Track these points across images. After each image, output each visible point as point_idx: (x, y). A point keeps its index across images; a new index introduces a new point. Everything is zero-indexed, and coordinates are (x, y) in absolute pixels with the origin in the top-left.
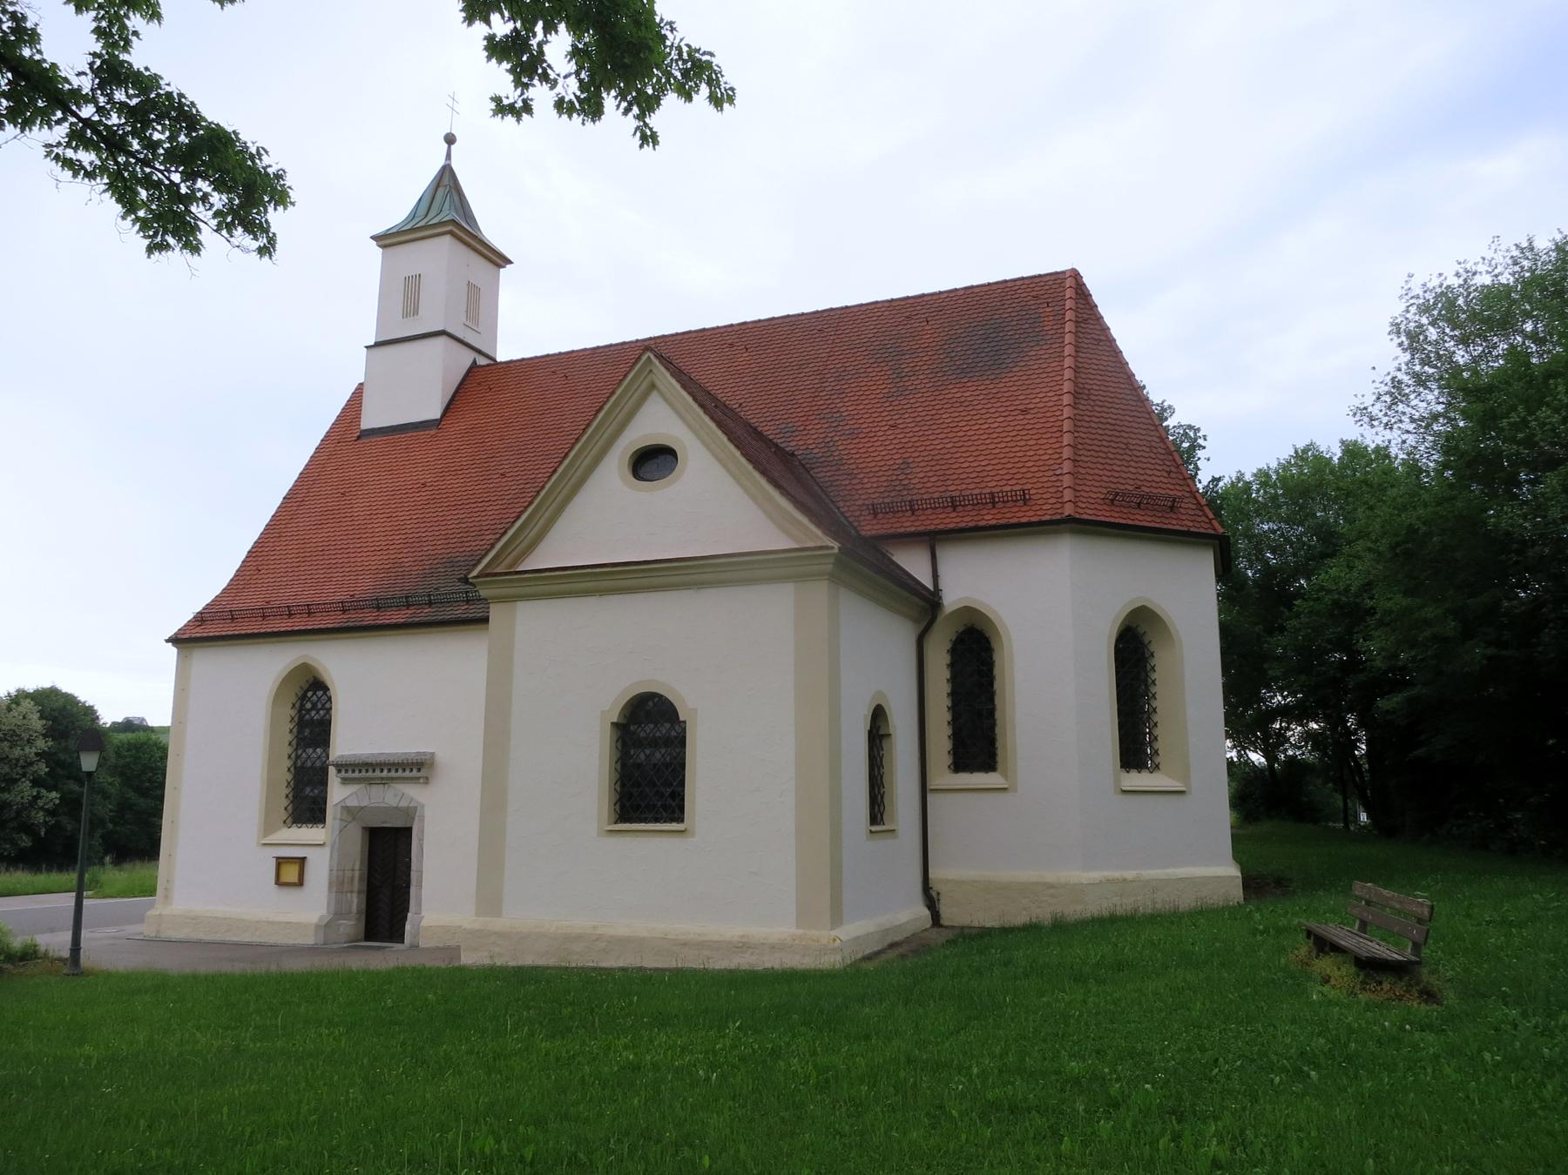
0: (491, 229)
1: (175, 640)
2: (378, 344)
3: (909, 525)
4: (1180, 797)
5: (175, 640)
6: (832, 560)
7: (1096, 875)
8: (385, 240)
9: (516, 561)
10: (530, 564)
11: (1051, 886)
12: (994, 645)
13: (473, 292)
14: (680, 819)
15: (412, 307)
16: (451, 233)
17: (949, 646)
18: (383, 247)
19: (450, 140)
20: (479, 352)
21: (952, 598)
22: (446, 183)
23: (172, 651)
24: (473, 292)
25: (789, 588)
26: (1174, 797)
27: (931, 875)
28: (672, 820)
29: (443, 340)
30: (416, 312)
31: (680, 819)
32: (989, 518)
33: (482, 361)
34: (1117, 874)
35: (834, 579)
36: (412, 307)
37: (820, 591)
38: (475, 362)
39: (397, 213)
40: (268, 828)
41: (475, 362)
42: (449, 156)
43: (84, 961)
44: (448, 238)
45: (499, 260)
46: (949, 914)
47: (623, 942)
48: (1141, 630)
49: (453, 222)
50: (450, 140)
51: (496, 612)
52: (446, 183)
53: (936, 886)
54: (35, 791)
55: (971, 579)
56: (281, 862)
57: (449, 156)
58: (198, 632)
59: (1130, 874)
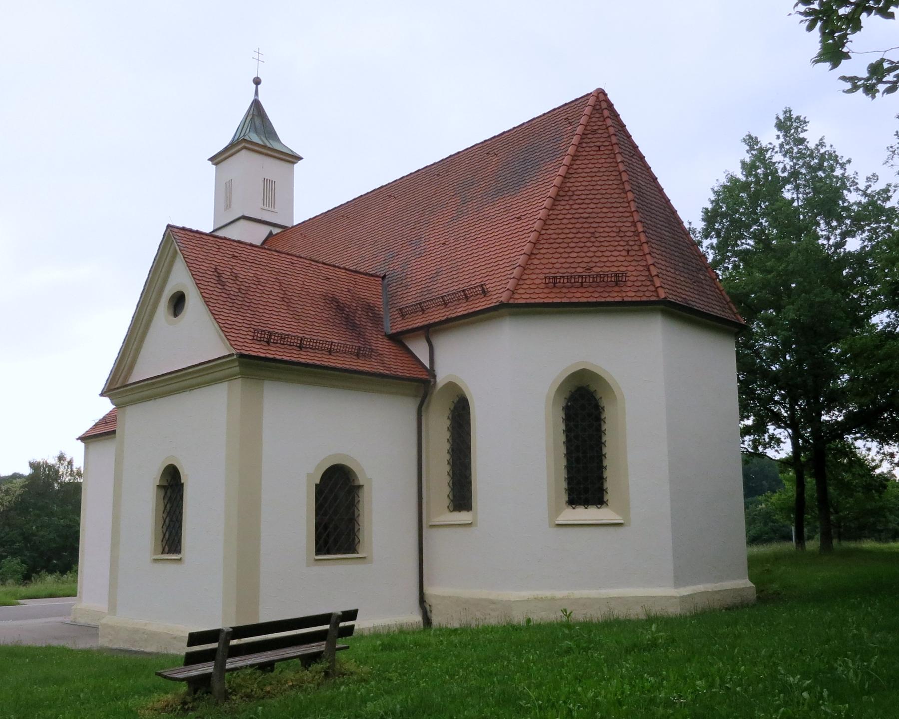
0: (288, 138)
1: (83, 438)
3: (418, 321)
4: (616, 528)
5: (83, 438)
6: (236, 364)
7: (526, 594)
8: (216, 159)
10: (130, 381)
12: (604, 403)
13: (269, 185)
15: (228, 205)
16: (245, 148)
17: (447, 412)
18: (216, 164)
19: (257, 82)
21: (442, 376)
23: (81, 445)
24: (269, 185)
26: (611, 529)
27: (427, 590)
29: (242, 221)
30: (230, 206)
33: (276, 231)
35: (244, 375)
36: (228, 205)
37: (238, 384)
38: (271, 233)
41: (271, 233)
44: (244, 152)
45: (292, 158)
46: (436, 620)
47: (153, 635)
50: (257, 82)
53: (429, 600)
54: (13, 531)
55: (458, 360)
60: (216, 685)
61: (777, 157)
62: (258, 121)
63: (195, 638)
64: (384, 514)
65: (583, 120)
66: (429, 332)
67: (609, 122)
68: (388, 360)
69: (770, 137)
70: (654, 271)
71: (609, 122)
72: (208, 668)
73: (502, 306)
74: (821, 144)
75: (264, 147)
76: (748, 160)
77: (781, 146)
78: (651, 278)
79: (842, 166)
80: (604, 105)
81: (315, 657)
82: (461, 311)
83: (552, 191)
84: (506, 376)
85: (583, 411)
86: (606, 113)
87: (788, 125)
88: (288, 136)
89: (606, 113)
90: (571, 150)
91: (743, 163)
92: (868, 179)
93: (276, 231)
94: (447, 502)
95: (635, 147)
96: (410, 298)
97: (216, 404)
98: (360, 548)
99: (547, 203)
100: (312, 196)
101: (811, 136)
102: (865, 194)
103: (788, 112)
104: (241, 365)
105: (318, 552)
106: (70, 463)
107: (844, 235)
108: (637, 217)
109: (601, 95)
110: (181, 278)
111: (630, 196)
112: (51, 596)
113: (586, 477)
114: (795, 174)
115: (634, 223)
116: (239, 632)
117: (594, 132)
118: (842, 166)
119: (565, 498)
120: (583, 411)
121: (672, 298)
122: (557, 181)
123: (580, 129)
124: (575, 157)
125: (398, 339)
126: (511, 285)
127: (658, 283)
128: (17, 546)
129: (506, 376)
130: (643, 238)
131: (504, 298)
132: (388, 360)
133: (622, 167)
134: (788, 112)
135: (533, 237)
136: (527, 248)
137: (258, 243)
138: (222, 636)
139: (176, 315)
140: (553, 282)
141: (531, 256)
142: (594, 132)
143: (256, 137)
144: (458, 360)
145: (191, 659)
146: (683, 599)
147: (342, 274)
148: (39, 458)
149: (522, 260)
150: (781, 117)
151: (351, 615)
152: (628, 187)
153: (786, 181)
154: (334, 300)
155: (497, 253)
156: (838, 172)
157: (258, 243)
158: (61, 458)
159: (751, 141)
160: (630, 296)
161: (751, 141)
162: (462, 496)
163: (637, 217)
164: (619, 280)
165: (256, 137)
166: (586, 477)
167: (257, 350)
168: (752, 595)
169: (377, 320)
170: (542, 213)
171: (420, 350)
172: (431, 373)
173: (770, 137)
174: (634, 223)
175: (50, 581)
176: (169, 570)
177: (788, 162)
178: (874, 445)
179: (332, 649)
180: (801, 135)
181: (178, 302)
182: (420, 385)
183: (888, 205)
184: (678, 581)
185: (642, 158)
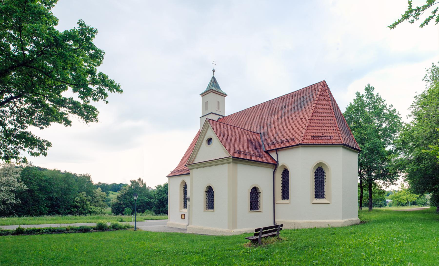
1: (168, 177)
2: (202, 117)
7: (304, 221)
8: (203, 95)
9: (193, 162)
11: (295, 223)
13: (218, 103)
14: (258, 209)
15: (207, 109)
17: (282, 173)
19: (214, 71)
20: (220, 115)
22: (214, 80)
23: (167, 178)
25: (227, 165)
27: (276, 220)
28: (211, 209)
31: (258, 209)
32: (287, 145)
33: (221, 117)
34: (310, 221)
35: (233, 162)
37: (231, 165)
39: (204, 89)
40: (180, 210)
42: (214, 74)
43: (137, 227)
45: (224, 95)
48: (322, 167)
49: (212, 89)
50: (214, 71)
51: (191, 172)
52: (214, 80)
55: (285, 159)
56: (182, 215)
57: (214, 74)
58: (171, 175)
59: (313, 221)
60: (260, 241)
61: (365, 99)
62: (215, 83)
63: (256, 230)
64: (265, 199)
65: (320, 90)
66: (277, 150)
67: (327, 91)
68: (266, 159)
69: (363, 92)
70: (340, 136)
71: (327, 91)
72: (257, 237)
73: (300, 144)
74: (377, 95)
75: (217, 91)
76: (356, 99)
77: (366, 95)
78: (339, 137)
79: (383, 102)
80: (326, 86)
81: (274, 235)
82: (287, 145)
83: (312, 111)
84: (300, 164)
85: (320, 174)
86: (326, 88)
87: (369, 89)
88: (223, 89)
89: (326, 88)
90: (317, 99)
91: (354, 100)
92: (390, 106)
93: (221, 117)
94: (281, 197)
95: (333, 98)
96: (270, 141)
97: (224, 170)
98: (260, 209)
99: (311, 115)
100: (231, 108)
101: (375, 93)
102: (389, 111)
103: (369, 85)
104: (233, 160)
105: (251, 210)
106: (142, 181)
107: (383, 122)
108: (335, 120)
109: (324, 82)
110: (210, 133)
111: (334, 113)
112: (152, 219)
113: (320, 191)
114: (369, 104)
115: (335, 121)
116: (265, 229)
117: (323, 94)
118: (383, 102)
119: (314, 196)
120: (320, 174)
121: (345, 143)
122: (313, 108)
123: (319, 93)
124: (318, 101)
125: (267, 152)
126: (302, 138)
127: (341, 139)
128: (128, 204)
129: (300, 164)
130: (337, 126)
131: (300, 142)
132: (266, 159)
133: (331, 105)
134: (369, 85)
135: (307, 125)
136: (306, 128)
137: (216, 120)
138: (261, 230)
139: (209, 144)
140: (314, 138)
141: (307, 130)
142: (323, 94)
143: (214, 89)
144: (285, 159)
145: (255, 235)
146: (344, 222)
147: (250, 133)
148: (133, 179)
149: (305, 131)
150: (367, 86)
151: (282, 225)
152: (333, 111)
153: (367, 106)
154: (250, 141)
155: (297, 128)
156: (382, 104)
157: (216, 120)
158: (140, 180)
159: (358, 94)
160: (334, 142)
161: (358, 94)
162: (286, 195)
163: (335, 120)
164: (331, 138)
165: (214, 89)
166: (320, 191)
167: (236, 155)
168: (359, 222)
169: (261, 146)
170: (309, 118)
171: (274, 155)
172: (277, 162)
173: (363, 92)
174: (335, 121)
175: (161, 216)
176: (210, 213)
177: (368, 101)
178: (382, 181)
179: (278, 233)
180: (372, 92)
181: (210, 141)
182: (275, 165)
183: (395, 114)
184: (343, 218)
185: (335, 102)
